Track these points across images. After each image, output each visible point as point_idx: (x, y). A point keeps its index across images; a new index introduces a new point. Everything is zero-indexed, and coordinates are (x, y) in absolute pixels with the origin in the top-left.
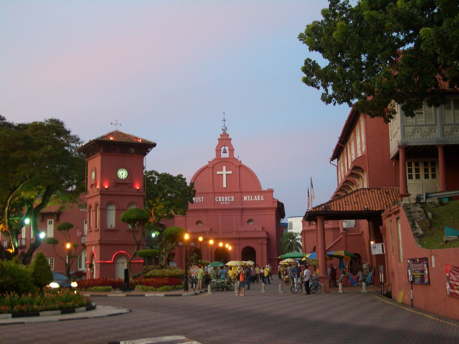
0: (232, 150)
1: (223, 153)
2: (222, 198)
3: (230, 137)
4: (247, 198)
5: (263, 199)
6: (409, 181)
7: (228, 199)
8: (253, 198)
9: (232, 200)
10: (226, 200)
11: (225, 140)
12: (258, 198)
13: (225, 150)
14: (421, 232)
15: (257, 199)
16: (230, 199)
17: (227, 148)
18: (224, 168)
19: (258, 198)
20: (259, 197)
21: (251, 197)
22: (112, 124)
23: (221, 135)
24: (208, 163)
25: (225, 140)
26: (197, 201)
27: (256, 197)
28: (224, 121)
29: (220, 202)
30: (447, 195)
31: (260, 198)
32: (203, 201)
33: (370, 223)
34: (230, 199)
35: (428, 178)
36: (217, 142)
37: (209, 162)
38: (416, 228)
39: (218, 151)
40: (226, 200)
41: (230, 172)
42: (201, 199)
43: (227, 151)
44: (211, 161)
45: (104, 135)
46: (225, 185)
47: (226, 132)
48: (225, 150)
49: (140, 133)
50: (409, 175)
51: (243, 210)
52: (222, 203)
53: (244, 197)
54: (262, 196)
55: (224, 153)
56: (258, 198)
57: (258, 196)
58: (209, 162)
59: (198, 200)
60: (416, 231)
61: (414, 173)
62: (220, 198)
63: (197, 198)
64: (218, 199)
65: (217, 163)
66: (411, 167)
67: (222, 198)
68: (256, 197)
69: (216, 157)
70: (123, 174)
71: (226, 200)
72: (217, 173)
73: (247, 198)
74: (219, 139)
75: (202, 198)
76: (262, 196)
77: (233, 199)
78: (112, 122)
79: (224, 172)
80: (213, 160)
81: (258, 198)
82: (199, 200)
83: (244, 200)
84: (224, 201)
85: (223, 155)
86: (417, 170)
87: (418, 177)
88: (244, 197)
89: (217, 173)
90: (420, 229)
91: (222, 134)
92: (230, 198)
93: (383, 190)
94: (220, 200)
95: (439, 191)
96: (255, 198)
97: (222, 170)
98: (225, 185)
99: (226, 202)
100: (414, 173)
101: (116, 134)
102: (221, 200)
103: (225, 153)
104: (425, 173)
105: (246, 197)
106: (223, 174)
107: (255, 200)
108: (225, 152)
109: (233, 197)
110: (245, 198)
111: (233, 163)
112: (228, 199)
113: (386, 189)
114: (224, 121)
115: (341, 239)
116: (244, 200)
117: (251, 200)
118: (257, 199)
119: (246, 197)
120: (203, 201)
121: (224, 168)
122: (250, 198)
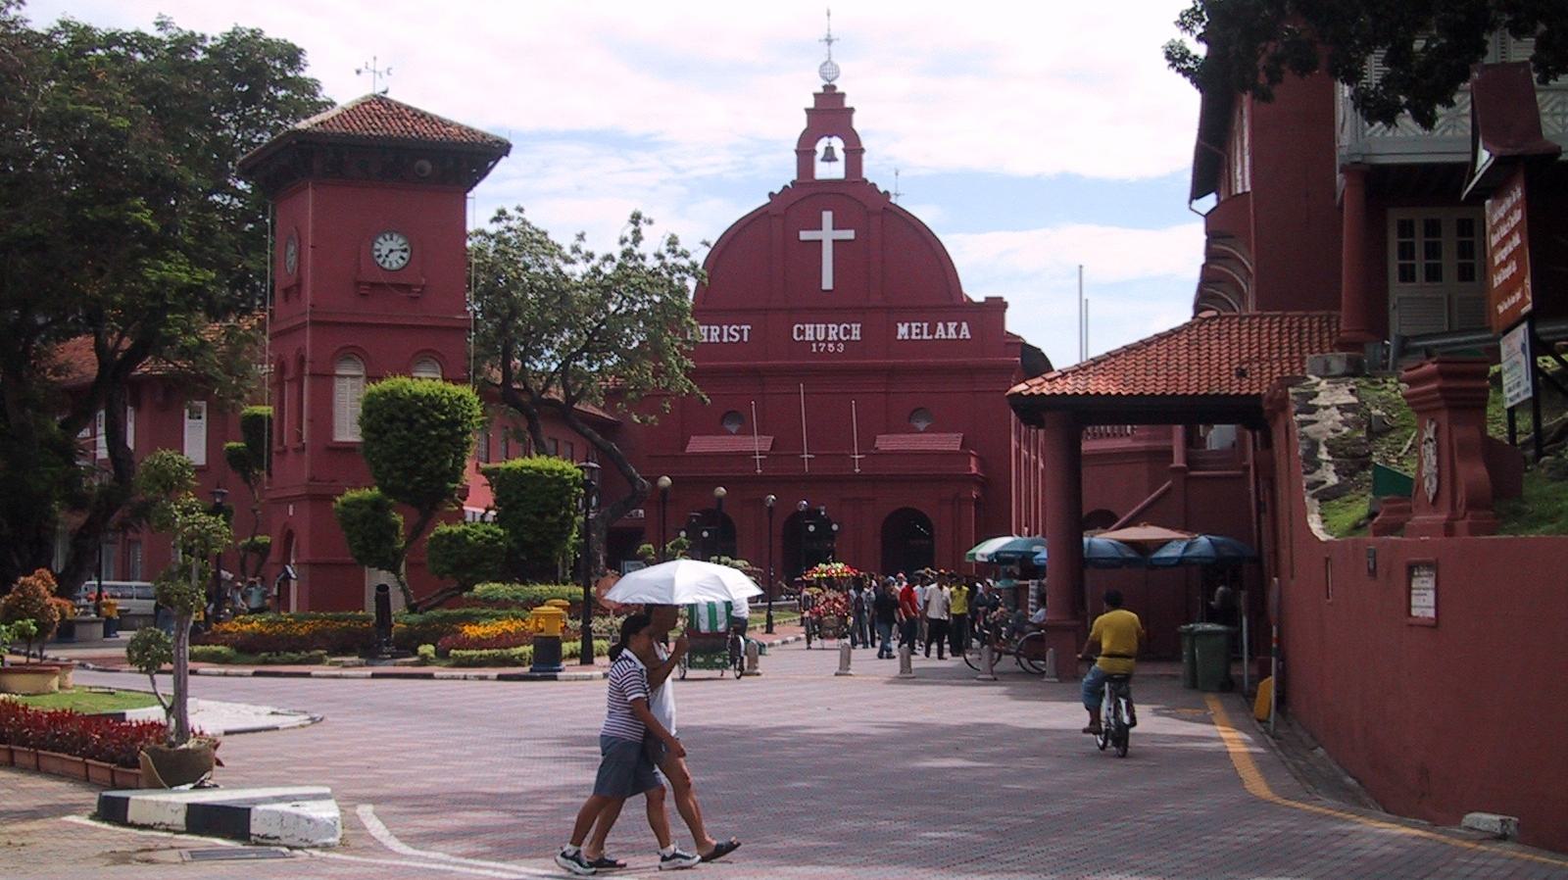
0: (854, 152)
1: (823, 160)
2: (815, 328)
3: (848, 104)
4: (910, 327)
5: (968, 337)
6: (1397, 290)
7: (838, 334)
8: (932, 331)
9: (853, 338)
10: (832, 336)
11: (830, 114)
12: (951, 330)
13: (829, 150)
14: (1332, 480)
15: (947, 334)
16: (848, 332)
17: (838, 144)
18: (827, 217)
19: (946, 331)
20: (952, 326)
21: (925, 325)
22: (358, 72)
23: (816, 95)
24: (768, 200)
25: (830, 114)
26: (725, 340)
27: (940, 326)
28: (829, 41)
29: (811, 342)
30: (1466, 343)
31: (958, 330)
32: (746, 339)
33: (1258, 434)
34: (848, 332)
35: (1413, 279)
36: (802, 123)
37: (771, 195)
38: (1318, 465)
39: (805, 152)
40: (832, 336)
41: (849, 234)
42: (741, 332)
43: (840, 154)
44: (777, 191)
45: (366, 97)
46: (827, 283)
47: (834, 83)
48: (829, 150)
49: (453, 99)
50: (1402, 268)
51: (891, 372)
52: (818, 348)
53: (899, 325)
54: (965, 325)
55: (827, 164)
56: (951, 330)
57: (950, 324)
58: (771, 195)
59: (729, 335)
60: (1317, 476)
61: (1420, 263)
62: (809, 329)
63: (725, 327)
64: (801, 332)
65: (802, 199)
66: (1411, 240)
67: (815, 328)
68: (940, 326)
69: (798, 177)
70: (391, 252)
71: (830, 338)
72: (853, 232)
73: (910, 327)
74: (808, 111)
75: (746, 328)
76: (965, 325)
77: (856, 335)
78: (357, 68)
79: (828, 234)
80: (786, 187)
81: (946, 331)
82: (734, 337)
83: (899, 337)
84: (825, 341)
85: (825, 171)
86: (1432, 251)
87: (1433, 274)
88: (899, 325)
89: (853, 232)
90: (1332, 467)
91: (821, 90)
92: (799, 329)
93: (1291, 323)
94: (809, 336)
95: (348, 381)
96: (940, 332)
97: (818, 226)
98: (827, 283)
99: (830, 345)
100: (1420, 263)
101: (380, 103)
102: (812, 339)
103: (829, 161)
104: (1402, 262)
105: (906, 325)
106: (821, 241)
107: (937, 337)
108: (829, 156)
109: (859, 326)
110: (903, 330)
111: (862, 203)
112: (838, 334)
113: (1303, 317)
114: (829, 41)
115: (1169, 489)
116: (899, 337)
117: (925, 337)
118: (947, 334)
119: (906, 325)
120: (746, 339)
121: (827, 217)
122: (922, 328)
